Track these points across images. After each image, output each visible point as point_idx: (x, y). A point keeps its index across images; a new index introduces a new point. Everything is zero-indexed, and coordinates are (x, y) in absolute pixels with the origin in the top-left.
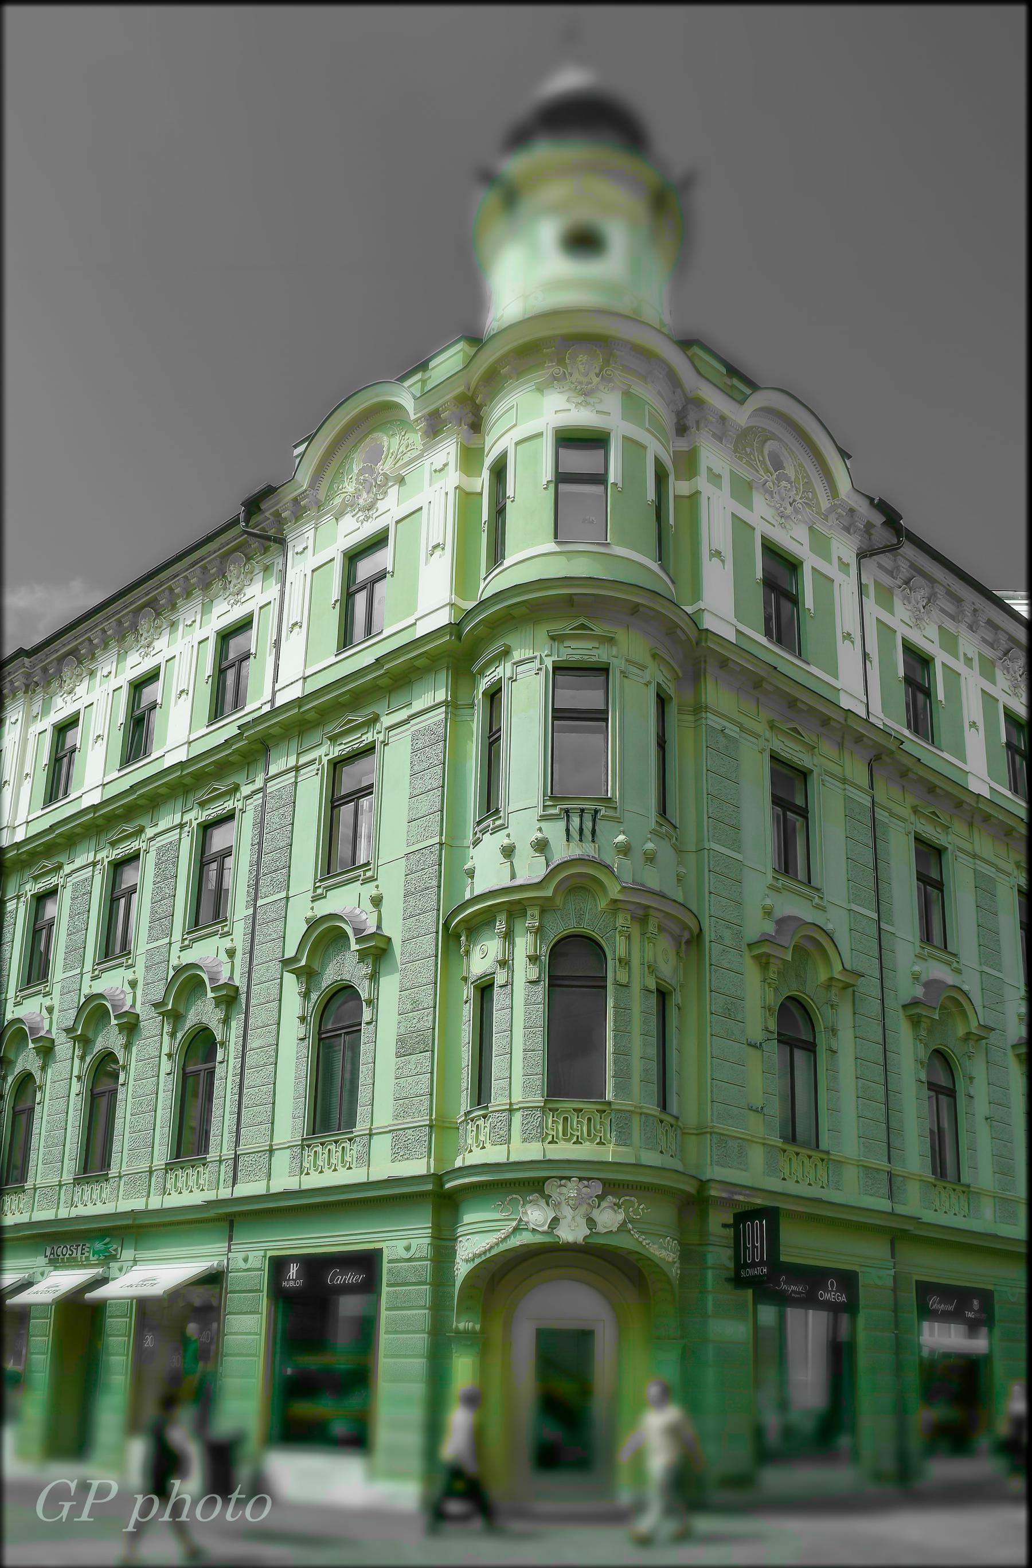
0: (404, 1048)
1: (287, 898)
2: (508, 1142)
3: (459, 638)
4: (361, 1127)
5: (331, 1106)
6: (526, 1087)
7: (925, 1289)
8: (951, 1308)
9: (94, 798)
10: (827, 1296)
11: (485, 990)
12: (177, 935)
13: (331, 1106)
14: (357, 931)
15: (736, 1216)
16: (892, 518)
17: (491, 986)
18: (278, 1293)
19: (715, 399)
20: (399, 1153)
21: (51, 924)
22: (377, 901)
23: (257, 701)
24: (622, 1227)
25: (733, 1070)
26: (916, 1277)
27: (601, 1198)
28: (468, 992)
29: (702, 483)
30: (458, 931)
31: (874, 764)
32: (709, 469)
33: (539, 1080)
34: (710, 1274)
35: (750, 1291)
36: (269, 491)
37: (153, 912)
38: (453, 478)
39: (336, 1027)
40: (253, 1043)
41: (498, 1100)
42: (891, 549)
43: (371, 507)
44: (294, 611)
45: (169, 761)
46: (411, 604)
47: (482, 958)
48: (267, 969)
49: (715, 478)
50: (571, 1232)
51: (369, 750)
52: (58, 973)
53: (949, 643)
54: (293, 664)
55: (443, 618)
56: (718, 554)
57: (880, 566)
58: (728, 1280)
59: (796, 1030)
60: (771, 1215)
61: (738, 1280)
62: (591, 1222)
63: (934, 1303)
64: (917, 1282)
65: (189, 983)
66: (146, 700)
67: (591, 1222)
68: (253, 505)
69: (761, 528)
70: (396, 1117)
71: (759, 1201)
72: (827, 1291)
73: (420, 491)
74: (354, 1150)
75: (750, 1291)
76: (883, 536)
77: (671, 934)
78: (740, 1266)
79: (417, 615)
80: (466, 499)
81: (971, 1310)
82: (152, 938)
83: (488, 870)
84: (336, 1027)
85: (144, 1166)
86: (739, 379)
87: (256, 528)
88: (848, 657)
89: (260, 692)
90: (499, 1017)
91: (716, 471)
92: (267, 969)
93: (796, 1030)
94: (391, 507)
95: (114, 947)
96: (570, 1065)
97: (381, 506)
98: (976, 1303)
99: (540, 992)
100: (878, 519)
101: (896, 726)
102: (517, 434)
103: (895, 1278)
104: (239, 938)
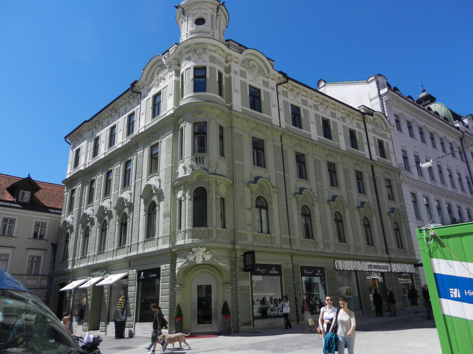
0: (165, 217)
1: (142, 180)
2: (185, 239)
3: (174, 117)
4: (156, 237)
5: (150, 232)
6: (188, 225)
7: (303, 268)
8: (311, 273)
9: (120, 146)
10: (272, 272)
11: (180, 201)
12: (120, 190)
13: (150, 232)
14: (155, 188)
15: (244, 253)
16: (285, 75)
17: (181, 201)
18: (139, 280)
19: (235, 54)
20: (164, 243)
21: (130, 170)
22: (160, 181)
23: (135, 133)
24: (212, 259)
25: (247, 216)
26: (300, 265)
27: (206, 252)
28: (178, 202)
29: (232, 74)
30: (175, 189)
31: (282, 136)
32: (234, 71)
33: (191, 223)
34: (238, 269)
35: (249, 272)
36: (136, 82)
37: (115, 184)
38: (174, 78)
39: (151, 211)
40: (134, 216)
41: (183, 229)
42: (286, 82)
43: (158, 85)
44: (143, 111)
45: (118, 147)
46: (166, 109)
47: (180, 194)
48: (137, 198)
49: (236, 73)
50: (199, 261)
51: (158, 144)
52: (95, 201)
53: (305, 102)
54: (143, 123)
55: (172, 112)
56: (237, 91)
57: (284, 87)
58: (243, 270)
59: (262, 204)
60: (252, 253)
61: (245, 270)
62: (204, 258)
63: (306, 272)
64: (301, 266)
65: (121, 201)
66: (157, 101)
67: (204, 258)
68: (133, 85)
69: (249, 83)
70: (163, 233)
71: (250, 249)
72: (272, 270)
73: (166, 83)
74: (155, 242)
75: (249, 272)
76: (283, 79)
77: (225, 185)
78: (245, 266)
79: (167, 111)
80: (177, 83)
81: (318, 273)
82: (115, 191)
83: (181, 174)
84: (151, 211)
85: (112, 249)
86: (241, 48)
87: (134, 91)
88: (274, 111)
89: (136, 129)
90: (183, 208)
91: (236, 71)
92: (137, 198)
93: (262, 204)
94: (162, 85)
95: (107, 192)
96: (200, 218)
97: (160, 84)
98: (319, 271)
99: (191, 202)
100: (281, 76)
101: (289, 125)
102: (186, 67)
103: (293, 266)
104: (132, 191)
